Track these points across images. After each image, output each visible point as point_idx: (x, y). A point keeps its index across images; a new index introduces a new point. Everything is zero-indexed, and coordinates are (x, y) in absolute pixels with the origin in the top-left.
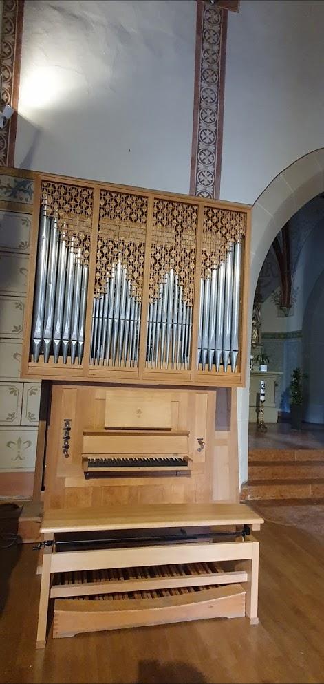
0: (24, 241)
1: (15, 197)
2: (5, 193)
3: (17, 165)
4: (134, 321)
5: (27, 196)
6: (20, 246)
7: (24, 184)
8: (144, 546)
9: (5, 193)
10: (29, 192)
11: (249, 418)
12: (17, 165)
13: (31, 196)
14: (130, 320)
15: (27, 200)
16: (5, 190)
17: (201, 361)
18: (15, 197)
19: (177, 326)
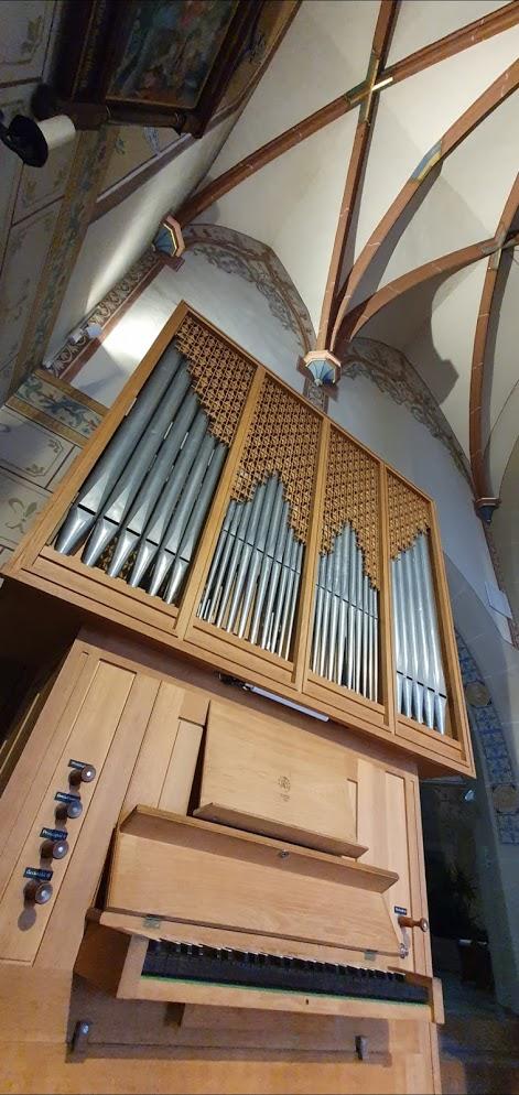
0: (39, 466)
1: (54, 412)
2: (41, 401)
3: (76, 383)
4: (176, 556)
5: (74, 419)
6: (28, 469)
7: (76, 407)
8: (328, 122)
9: (41, 401)
10: (80, 419)
11: (194, 1006)
12: (76, 383)
13: (79, 423)
14: (122, 528)
15: (70, 423)
16: (42, 397)
17: (403, 711)
18: (54, 412)
19: (137, 548)
